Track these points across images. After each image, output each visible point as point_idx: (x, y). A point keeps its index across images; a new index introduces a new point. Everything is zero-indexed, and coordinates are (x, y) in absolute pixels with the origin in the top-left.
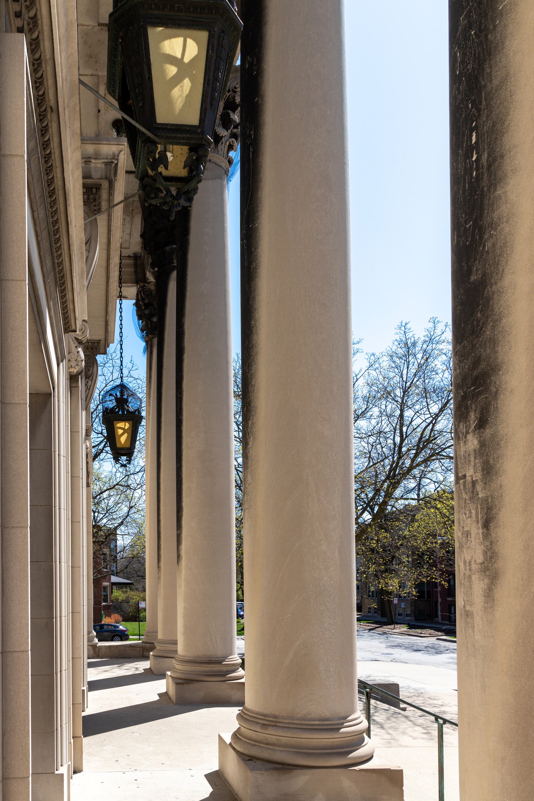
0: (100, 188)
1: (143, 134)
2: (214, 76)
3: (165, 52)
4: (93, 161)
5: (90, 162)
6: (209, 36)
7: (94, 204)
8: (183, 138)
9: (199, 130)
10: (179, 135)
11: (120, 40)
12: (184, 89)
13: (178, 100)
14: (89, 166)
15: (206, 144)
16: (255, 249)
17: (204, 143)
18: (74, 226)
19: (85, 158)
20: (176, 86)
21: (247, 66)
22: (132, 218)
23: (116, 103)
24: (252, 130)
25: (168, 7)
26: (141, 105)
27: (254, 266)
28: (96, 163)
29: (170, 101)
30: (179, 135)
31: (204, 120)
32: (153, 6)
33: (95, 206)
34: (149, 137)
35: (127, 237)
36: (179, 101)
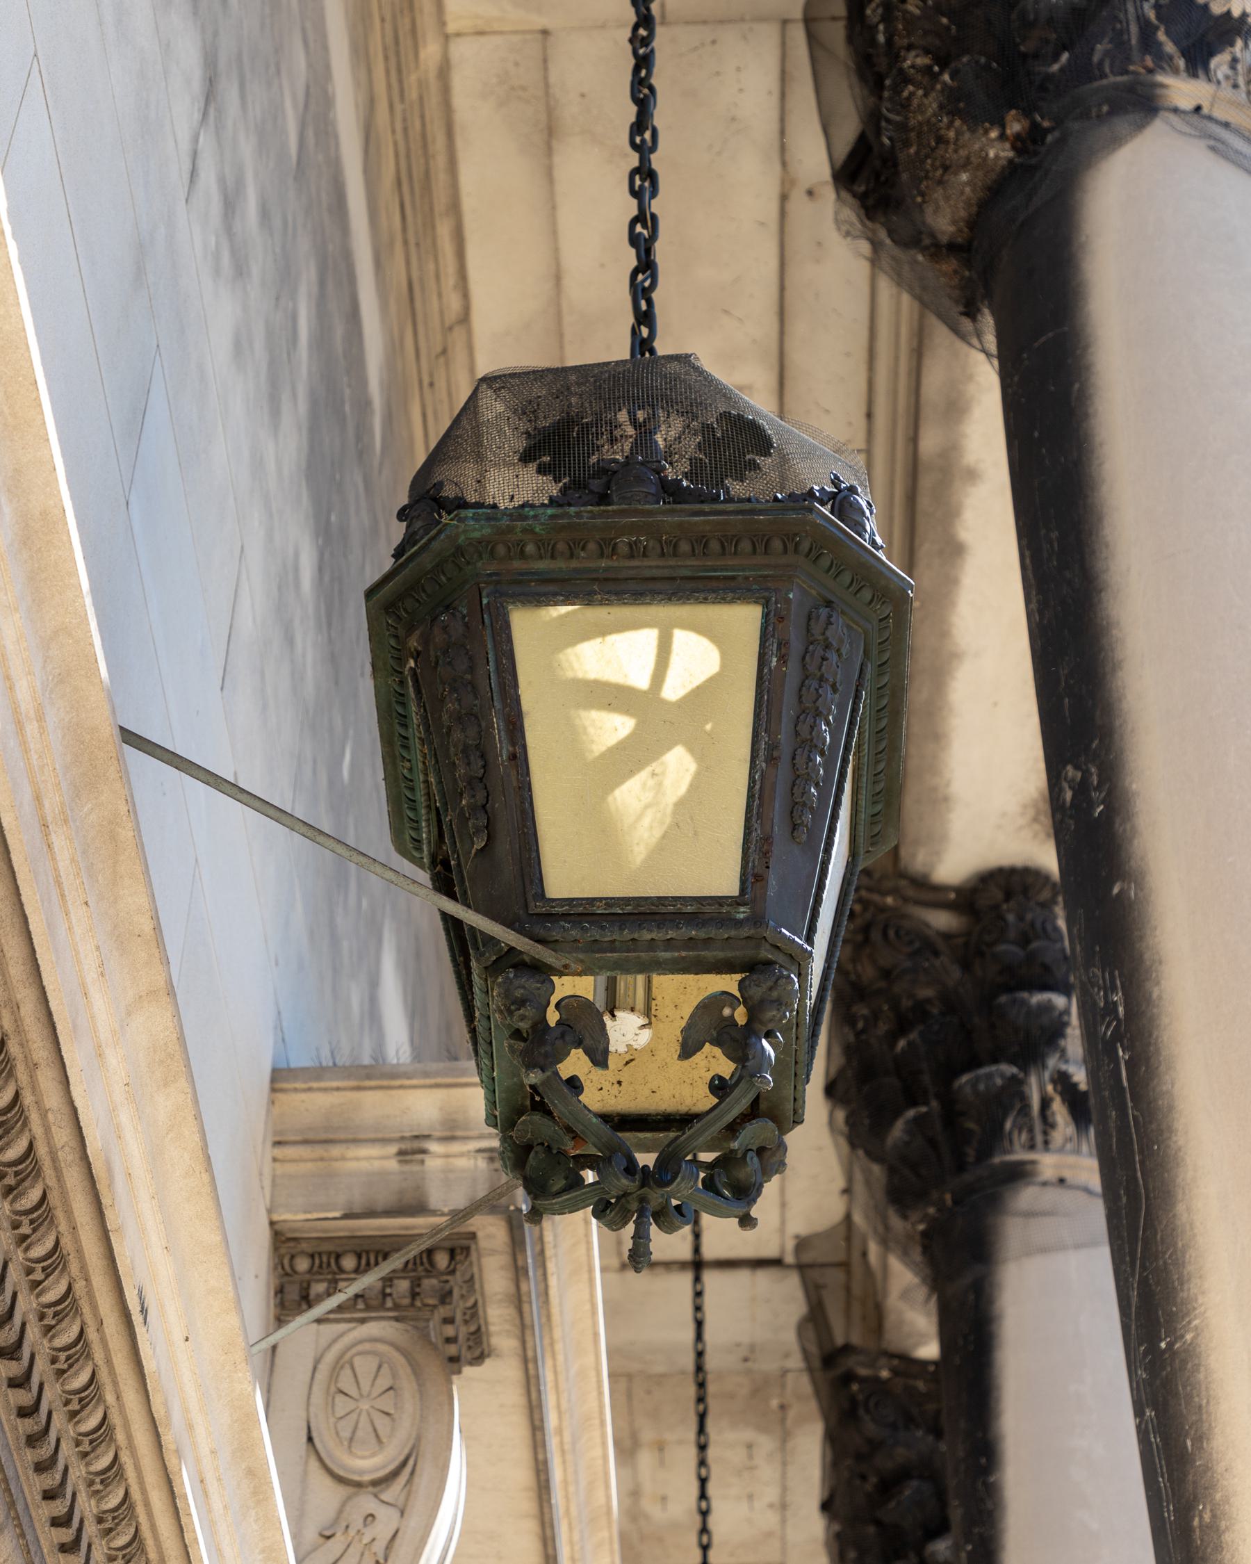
0: (466, 1250)
1: (490, 940)
2: (797, 733)
3: (580, 675)
4: (434, 1147)
5: (424, 1152)
6: (766, 616)
7: (443, 1311)
8: (669, 944)
9: (742, 913)
10: (647, 936)
11: (412, 663)
12: (667, 783)
13: (640, 817)
14: (416, 1168)
15: (780, 958)
16: (1199, 1439)
17: (766, 954)
18: (178, 1336)
19: (403, 1138)
20: (632, 773)
21: (1069, 795)
22: (785, 1437)
23: (424, 877)
24: (1113, 988)
25: (592, 546)
26: (479, 844)
27: (1207, 1517)
28: (447, 1156)
29: (606, 831)
30: (647, 936)
31: (759, 878)
32: (530, 548)
33: (449, 1321)
34: (512, 949)
35: (771, 1520)
36: (646, 821)
